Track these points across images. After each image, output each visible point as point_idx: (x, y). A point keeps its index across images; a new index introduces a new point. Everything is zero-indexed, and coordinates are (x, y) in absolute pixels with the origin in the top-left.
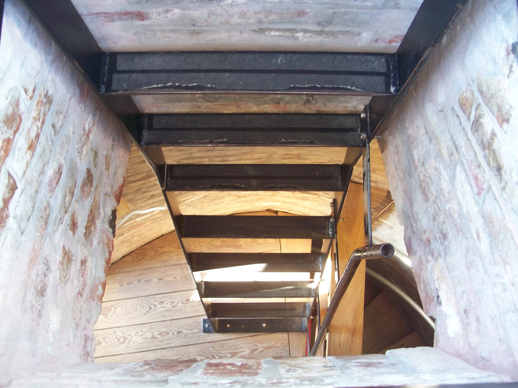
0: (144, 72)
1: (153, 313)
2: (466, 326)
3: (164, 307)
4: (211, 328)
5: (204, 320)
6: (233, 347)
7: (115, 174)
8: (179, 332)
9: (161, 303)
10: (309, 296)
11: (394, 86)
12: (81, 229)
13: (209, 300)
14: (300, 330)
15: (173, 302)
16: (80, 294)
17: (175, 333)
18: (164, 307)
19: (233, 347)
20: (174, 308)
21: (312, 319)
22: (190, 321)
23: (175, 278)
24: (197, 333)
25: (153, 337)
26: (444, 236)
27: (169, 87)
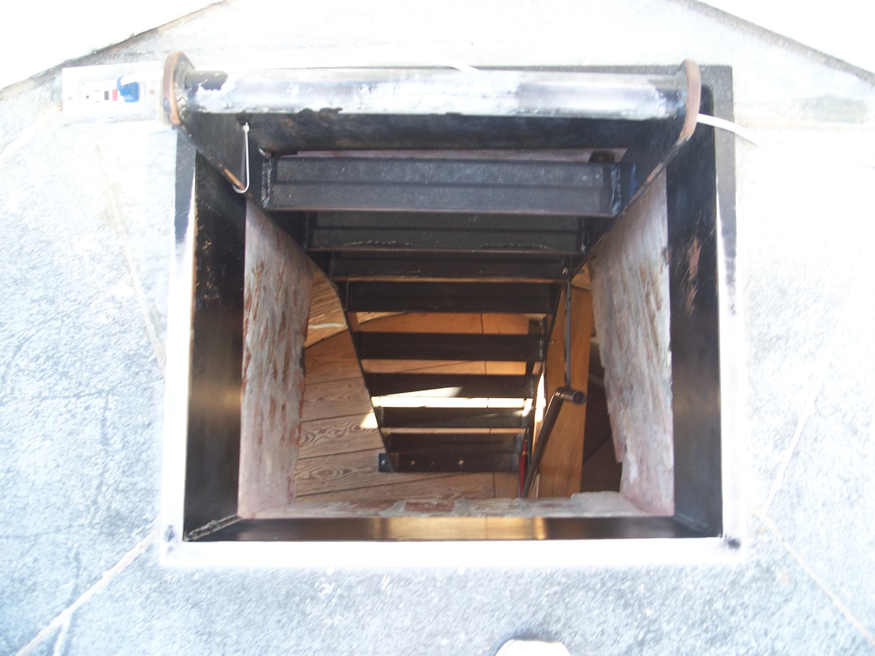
0: (344, 228)
1: (310, 445)
2: (641, 473)
3: (325, 437)
4: (390, 465)
5: (381, 456)
6: (419, 492)
7: (302, 308)
8: (346, 471)
9: (322, 431)
10: (519, 426)
11: (585, 244)
12: (280, 376)
13: (389, 431)
14: (510, 470)
15: (338, 431)
16: (283, 438)
17: (341, 472)
18: (325, 437)
19: (419, 492)
20: (339, 439)
21: (526, 457)
22: (360, 456)
23: (341, 397)
24: (371, 472)
25: (311, 478)
26: (631, 387)
27: (369, 245)
